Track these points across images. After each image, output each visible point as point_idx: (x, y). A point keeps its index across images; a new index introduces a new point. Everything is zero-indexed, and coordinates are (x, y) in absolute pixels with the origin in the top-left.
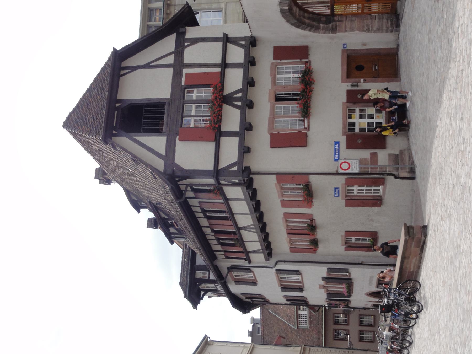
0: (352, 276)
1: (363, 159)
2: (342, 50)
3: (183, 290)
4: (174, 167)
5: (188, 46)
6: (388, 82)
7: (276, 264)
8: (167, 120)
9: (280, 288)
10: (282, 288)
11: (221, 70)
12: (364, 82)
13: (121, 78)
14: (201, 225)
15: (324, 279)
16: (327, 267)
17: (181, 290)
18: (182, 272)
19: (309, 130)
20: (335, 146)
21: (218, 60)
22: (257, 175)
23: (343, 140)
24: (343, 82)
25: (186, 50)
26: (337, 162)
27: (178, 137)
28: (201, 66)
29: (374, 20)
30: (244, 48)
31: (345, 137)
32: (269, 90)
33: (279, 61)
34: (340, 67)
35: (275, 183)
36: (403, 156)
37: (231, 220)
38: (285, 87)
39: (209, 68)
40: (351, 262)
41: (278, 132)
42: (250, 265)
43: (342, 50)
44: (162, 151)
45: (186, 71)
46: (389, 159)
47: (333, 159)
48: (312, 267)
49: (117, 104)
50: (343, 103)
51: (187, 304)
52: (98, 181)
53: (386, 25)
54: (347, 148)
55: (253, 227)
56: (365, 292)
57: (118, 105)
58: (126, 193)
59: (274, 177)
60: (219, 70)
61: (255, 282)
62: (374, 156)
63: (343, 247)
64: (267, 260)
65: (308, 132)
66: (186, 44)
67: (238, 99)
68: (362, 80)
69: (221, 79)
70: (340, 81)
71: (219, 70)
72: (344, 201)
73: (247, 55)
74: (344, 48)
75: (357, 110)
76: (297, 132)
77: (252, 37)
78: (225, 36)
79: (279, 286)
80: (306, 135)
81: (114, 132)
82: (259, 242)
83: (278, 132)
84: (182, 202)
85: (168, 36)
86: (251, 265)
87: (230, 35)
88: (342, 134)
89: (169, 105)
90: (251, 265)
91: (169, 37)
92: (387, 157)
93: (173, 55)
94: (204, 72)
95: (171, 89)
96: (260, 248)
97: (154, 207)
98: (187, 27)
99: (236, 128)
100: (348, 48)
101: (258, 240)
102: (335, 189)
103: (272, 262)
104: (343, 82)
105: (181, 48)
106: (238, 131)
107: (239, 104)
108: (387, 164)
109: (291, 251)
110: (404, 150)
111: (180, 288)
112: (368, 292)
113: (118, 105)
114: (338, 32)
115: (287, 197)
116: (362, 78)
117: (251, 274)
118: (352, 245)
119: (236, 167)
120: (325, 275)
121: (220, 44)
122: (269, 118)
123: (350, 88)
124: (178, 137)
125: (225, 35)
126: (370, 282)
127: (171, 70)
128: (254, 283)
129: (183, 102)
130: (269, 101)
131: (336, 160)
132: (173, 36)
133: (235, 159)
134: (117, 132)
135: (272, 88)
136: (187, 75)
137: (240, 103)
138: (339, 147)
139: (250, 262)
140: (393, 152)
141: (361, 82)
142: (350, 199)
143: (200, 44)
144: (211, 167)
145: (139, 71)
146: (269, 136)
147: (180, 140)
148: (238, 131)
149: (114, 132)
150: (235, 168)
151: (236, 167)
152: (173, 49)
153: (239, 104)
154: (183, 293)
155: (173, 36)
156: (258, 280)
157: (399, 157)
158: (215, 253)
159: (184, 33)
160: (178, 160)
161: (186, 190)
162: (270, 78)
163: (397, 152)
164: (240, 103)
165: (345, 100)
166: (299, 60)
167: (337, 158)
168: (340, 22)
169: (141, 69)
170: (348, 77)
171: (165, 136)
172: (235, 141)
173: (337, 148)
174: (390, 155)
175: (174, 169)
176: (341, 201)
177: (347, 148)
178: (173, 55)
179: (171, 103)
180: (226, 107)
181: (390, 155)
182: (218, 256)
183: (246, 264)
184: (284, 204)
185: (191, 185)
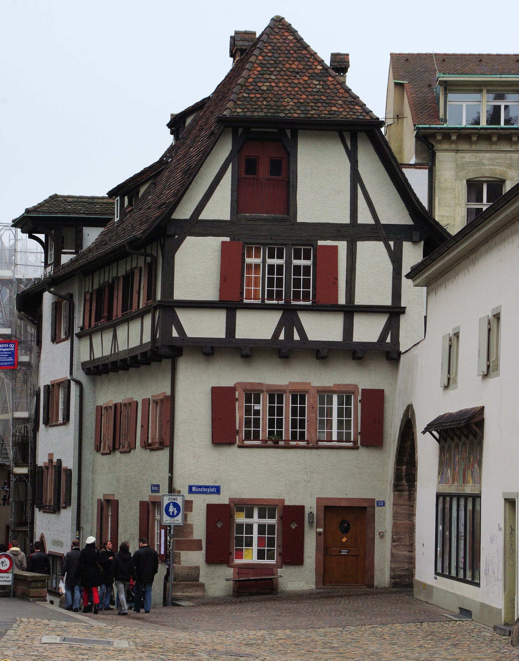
0: (63, 511)
1: (192, 528)
2: (375, 499)
3: (41, 205)
4: (178, 235)
5: (388, 247)
6: (316, 570)
7: (78, 383)
8: (258, 220)
9: (49, 384)
10: (48, 386)
11: (342, 306)
12: (317, 532)
13: (336, 134)
14: (119, 262)
15: (59, 461)
16: (72, 469)
17: (41, 200)
18: (75, 199)
19: (239, 447)
20: (212, 487)
21: (360, 300)
22: (172, 365)
23: (222, 499)
24: (318, 499)
25: (380, 245)
26: (187, 490)
27: (227, 239)
28: (351, 270)
29: (407, 549)
30: (378, 341)
31: (227, 502)
32: (310, 384)
33: (359, 398)
34: (344, 496)
35: (165, 393)
36: (194, 589)
37: (122, 315)
38: (313, 408)
39: (347, 284)
40: (82, 510)
41: (237, 399)
42: (74, 335)
43: (375, 499)
44: (204, 216)
45: (342, 246)
46: (191, 568)
47: (192, 484)
48: (72, 443)
49: (290, 130)
50: (283, 501)
51: (19, 212)
52: (233, 35)
53: (398, 568)
54: (208, 505)
55: (117, 351)
56: (44, 532)
57: (288, 132)
58: (197, 104)
59: (169, 393)
60: (342, 300)
61: (55, 340)
62: (196, 545)
63: (102, 498)
64: (84, 364)
65: (236, 445)
66: (391, 243)
67: (289, 335)
68: (321, 530)
69: (324, 306)
70: (318, 496)
71: (342, 300)
72: (146, 499)
73: (366, 347)
74: (378, 502)
75: (273, 521)
76: (237, 428)
77: (400, 354)
78: (400, 310)
79: (51, 382)
80: (231, 443)
81: (240, 131)
82: (89, 359)
83: (237, 399)
84: (126, 250)
85: (408, 211)
86: (75, 339)
87: (403, 319)
88: (232, 497)
89: (283, 220)
90: (75, 339)
91: (406, 212)
92: (193, 565)
93: (373, 222)
94: (339, 279)
95: (312, 222)
96: (96, 357)
97: (159, 170)
98: (422, 243)
99: (241, 333)
100: (377, 509)
101: (103, 355)
102: (158, 486)
103: (80, 375)
104: (318, 499)
105: (385, 235)
106: (237, 337)
107: (282, 337)
108: (183, 564)
109: (97, 407)
110: (204, 591)
111: (46, 197)
112: (44, 539)
113: (288, 132)
114: (394, 495)
115: (153, 410)
116: (324, 530)
117: (63, 336)
118: (105, 510)
119: (178, 336)
120: (64, 465)
121: (388, 302)
122: (261, 384)
123: (307, 511)
124: (227, 239)
125: (403, 311)
126: (56, 542)
127: (347, 220)
128: (55, 339)
129: (288, 244)
130: (290, 383)
131: (190, 487)
132: (408, 221)
133: (190, 333)
134: (241, 135)
135: (313, 387)
136: (336, 248)
137: (283, 339)
138: (211, 493)
139: (80, 336)
140: (202, 573)
141: (317, 528)
142: (148, 508)
143: (390, 267)
144: (179, 295)
145: (347, 164)
146: (232, 385)
147: (223, 243)
148: (237, 337)
149: (240, 131)
150: (175, 334)
151: (178, 336)
152: (383, 221)
153: (282, 337)
154: (35, 204)
155: (408, 221)
156: (59, 345)
157: (194, 583)
158: (91, 275)
159: (410, 239)
160: (190, 240)
161: (146, 255)
162: (331, 384)
163: (201, 580)
164: (283, 339)
165: (287, 503)
166: (359, 431)
167: (194, 489)
168: (407, 497)
169: (351, 168)
170: (327, 508)
171: (231, 218)
172: (220, 333)
173: (209, 490)
174: (197, 568)
175: (176, 237)
176: (146, 496)
177: (208, 505)
178: (373, 222)
179: (288, 223)
180: (275, 317)
181: (197, 568)
182: (88, 278)
183: (77, 330)
184: (146, 402)
185: (155, 260)
